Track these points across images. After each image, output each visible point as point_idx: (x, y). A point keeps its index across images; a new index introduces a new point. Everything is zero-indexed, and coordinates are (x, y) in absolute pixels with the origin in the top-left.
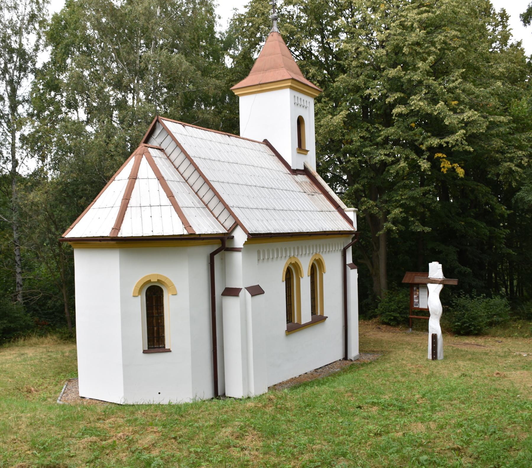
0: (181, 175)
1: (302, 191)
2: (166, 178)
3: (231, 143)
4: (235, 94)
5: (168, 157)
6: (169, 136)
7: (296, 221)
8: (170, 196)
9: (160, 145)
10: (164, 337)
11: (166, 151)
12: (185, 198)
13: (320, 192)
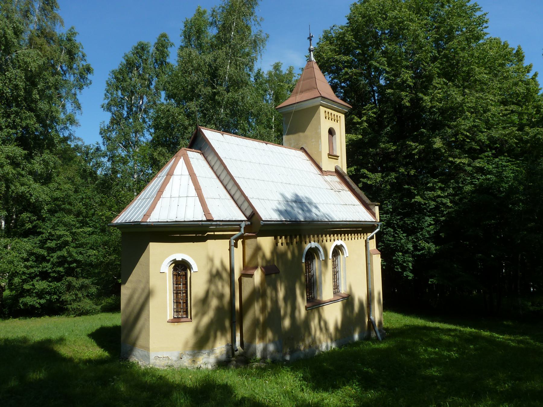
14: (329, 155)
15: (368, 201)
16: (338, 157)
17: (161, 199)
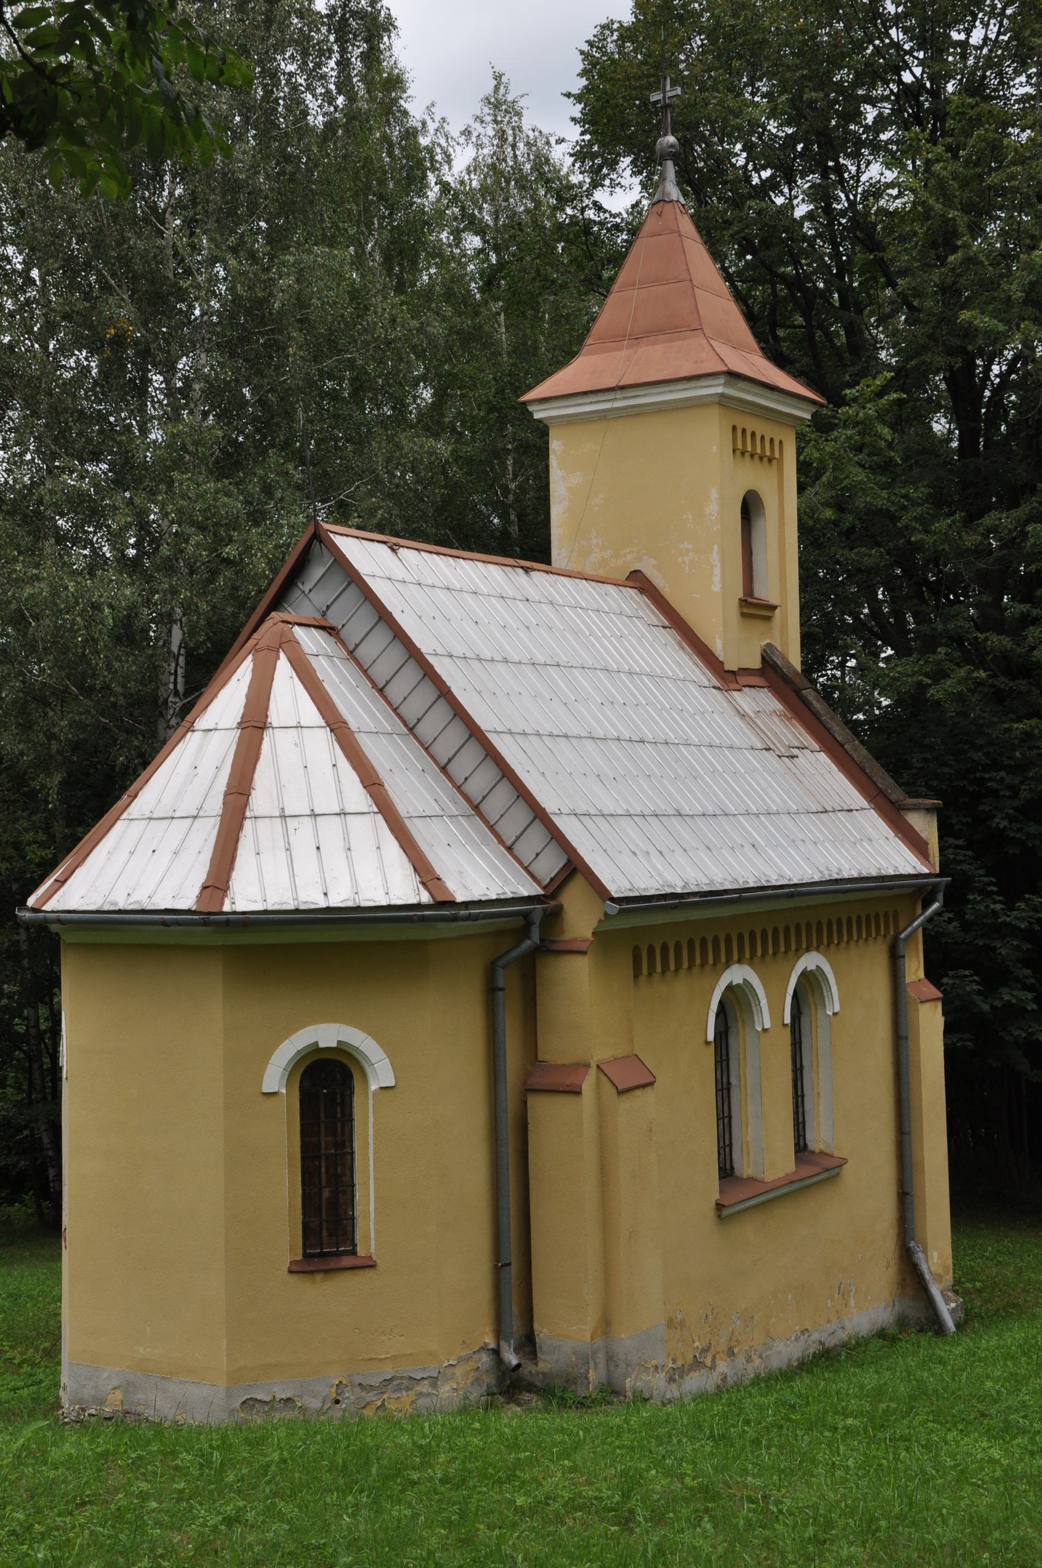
0: (395, 710)
1: (759, 745)
2: (353, 725)
3: (534, 595)
4: (537, 416)
5: (351, 653)
6: (353, 588)
7: (748, 849)
8: (371, 782)
9: (324, 614)
10: (353, 1218)
11: (343, 634)
12: (415, 790)
13: (817, 747)
14: (744, 603)
15: (897, 794)
16: (773, 608)
17: (248, 824)
